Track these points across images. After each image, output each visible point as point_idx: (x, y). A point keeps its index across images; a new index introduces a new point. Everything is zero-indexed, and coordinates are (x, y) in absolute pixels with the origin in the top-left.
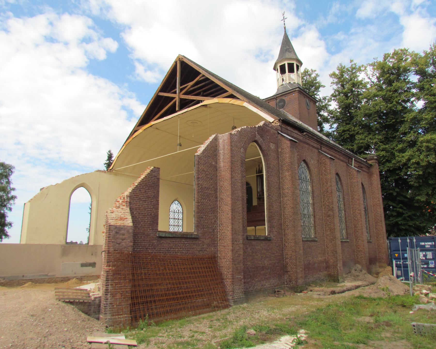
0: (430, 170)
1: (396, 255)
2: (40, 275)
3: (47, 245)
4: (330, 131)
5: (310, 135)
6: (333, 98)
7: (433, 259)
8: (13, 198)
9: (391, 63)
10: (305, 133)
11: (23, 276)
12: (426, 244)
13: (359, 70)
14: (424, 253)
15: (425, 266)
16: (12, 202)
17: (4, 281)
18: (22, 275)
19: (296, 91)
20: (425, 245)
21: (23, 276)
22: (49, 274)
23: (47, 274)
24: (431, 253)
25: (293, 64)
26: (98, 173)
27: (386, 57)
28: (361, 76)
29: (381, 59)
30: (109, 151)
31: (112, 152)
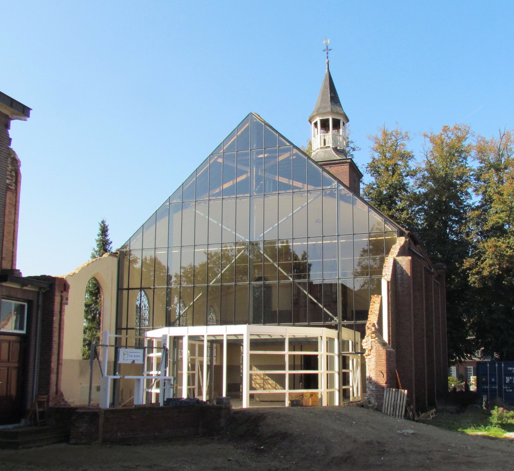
1: (484, 379)
9: (450, 138)
10: (418, 246)
13: (406, 137)
14: (511, 378)
19: (346, 162)
27: (446, 129)
28: (409, 147)
30: (103, 222)
31: (107, 224)
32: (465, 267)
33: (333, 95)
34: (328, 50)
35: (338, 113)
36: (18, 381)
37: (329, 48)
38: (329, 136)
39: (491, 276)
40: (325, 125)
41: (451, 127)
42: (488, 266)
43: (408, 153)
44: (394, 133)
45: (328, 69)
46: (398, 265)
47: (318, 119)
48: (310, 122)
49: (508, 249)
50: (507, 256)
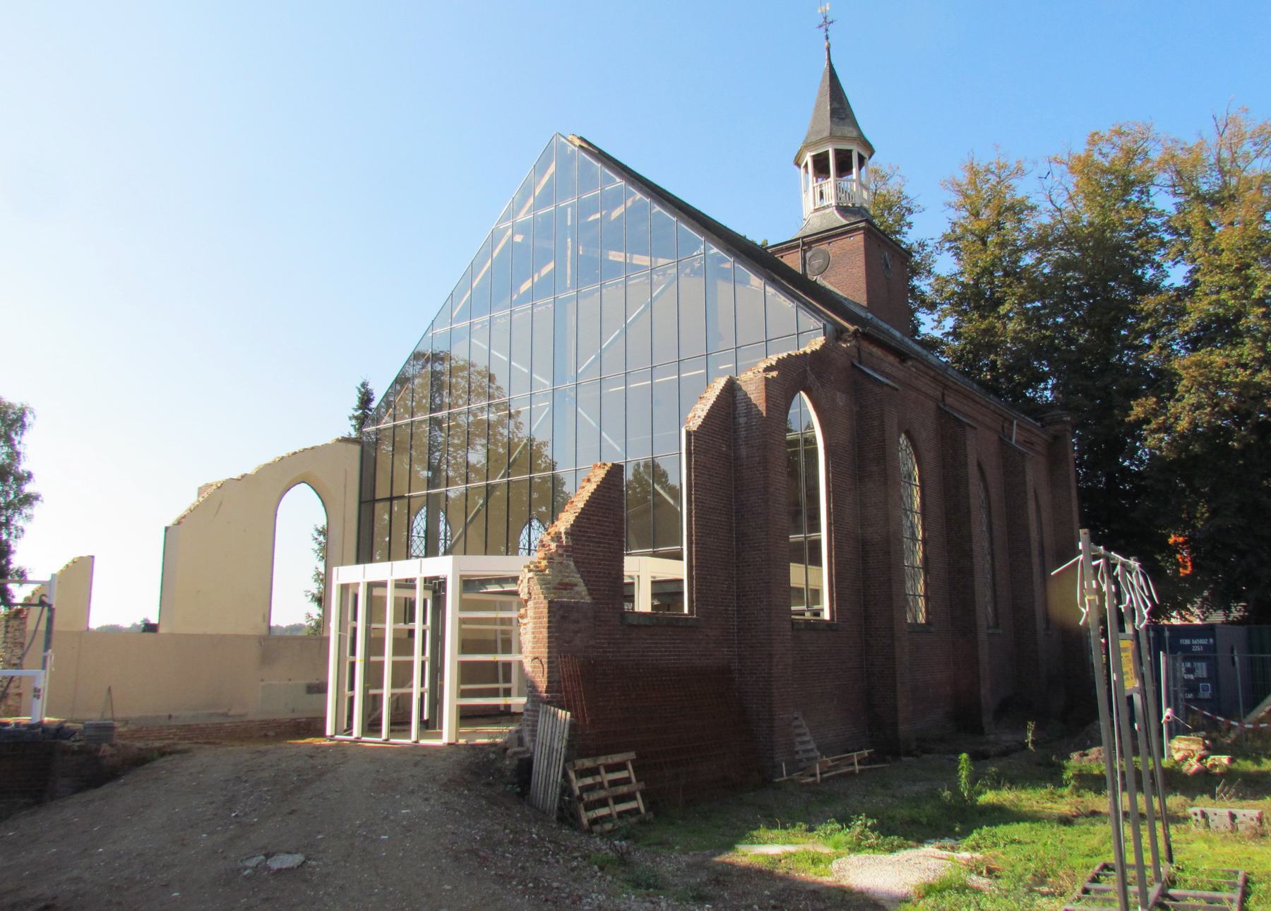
0: (1196, 448)
2: (211, 715)
3: (224, 636)
4: (937, 334)
5: (922, 367)
6: (947, 245)
7: (1208, 679)
8: (29, 500)
9: (1109, 155)
10: (910, 363)
11: (170, 717)
12: (1195, 642)
13: (1019, 172)
14: (1189, 665)
15: (1190, 696)
16: (26, 510)
17: (125, 729)
18: (167, 714)
19: (858, 229)
20: (1191, 646)
21: (170, 717)
22: (231, 713)
23: (226, 710)
24: (1204, 665)
25: (851, 151)
26: (343, 445)
27: (1094, 139)
28: (1023, 189)
29: (1080, 149)
30: (364, 385)
32: (1132, 418)
33: (836, 105)
34: (826, 23)
35: (844, 138)
36: (442, 679)
37: (829, 20)
38: (829, 185)
39: (1193, 433)
40: (820, 166)
41: (1106, 133)
42: (1186, 411)
43: (1021, 202)
44: (992, 168)
45: (829, 58)
46: (739, 394)
47: (808, 158)
48: (798, 165)
49: (1240, 371)
50: (1235, 384)
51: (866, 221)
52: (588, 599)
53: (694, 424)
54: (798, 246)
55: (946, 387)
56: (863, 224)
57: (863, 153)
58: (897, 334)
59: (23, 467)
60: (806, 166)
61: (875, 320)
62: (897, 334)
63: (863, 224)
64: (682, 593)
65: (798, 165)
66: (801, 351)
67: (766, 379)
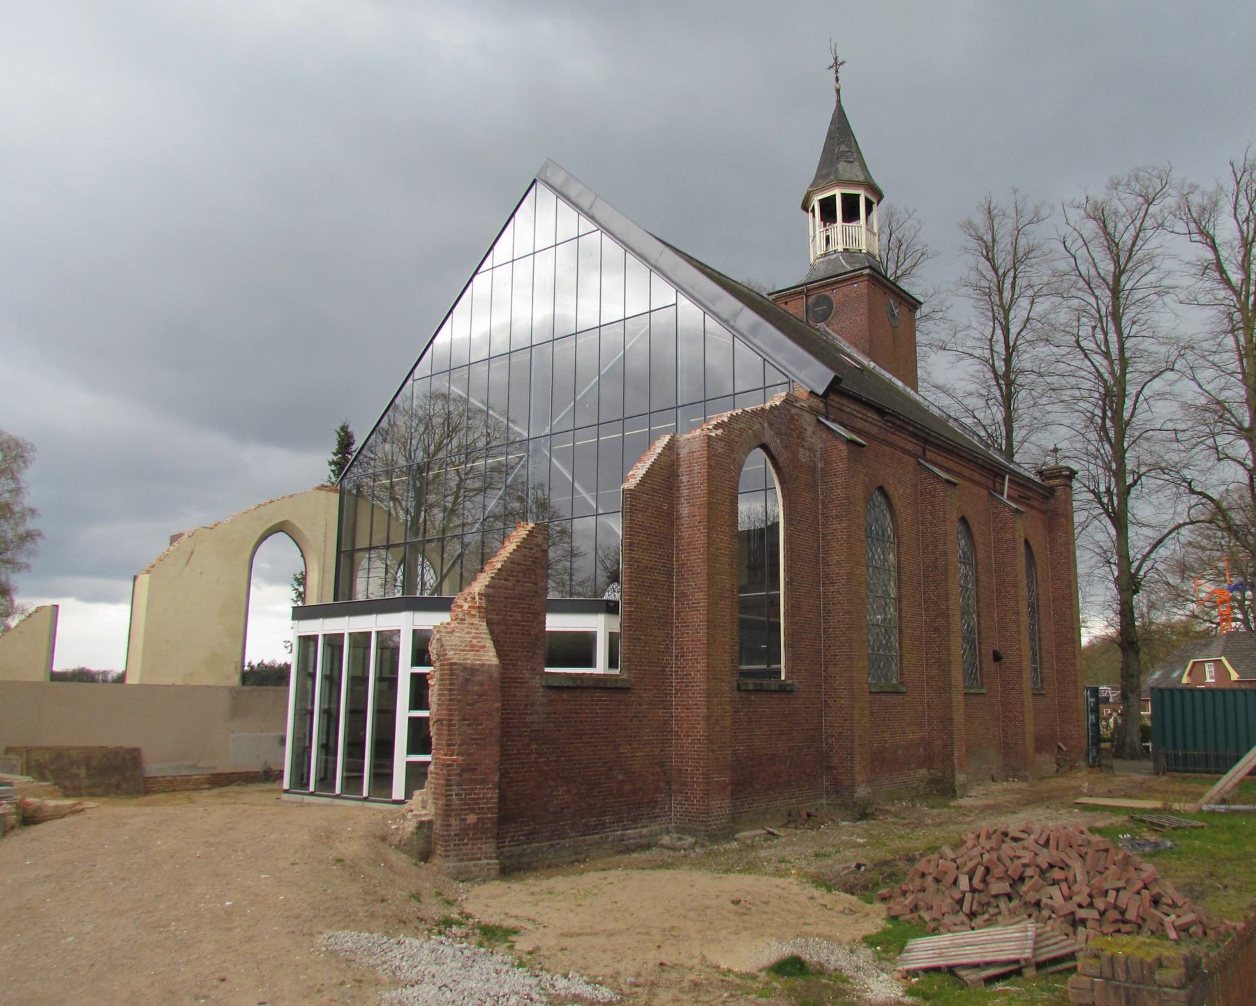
5: (898, 422)
8: (29, 536)
25: (858, 196)
30: (344, 428)
34: (836, 65)
37: (840, 60)
45: (839, 101)
47: (815, 203)
51: (870, 267)
52: (495, 661)
53: (631, 484)
54: (801, 293)
55: (926, 441)
56: (867, 271)
57: (871, 198)
58: (899, 384)
59: (28, 501)
60: (813, 210)
61: (878, 369)
62: (899, 384)
63: (867, 271)
64: (367, 679)
65: (807, 211)
66: (767, 406)
67: (709, 437)
